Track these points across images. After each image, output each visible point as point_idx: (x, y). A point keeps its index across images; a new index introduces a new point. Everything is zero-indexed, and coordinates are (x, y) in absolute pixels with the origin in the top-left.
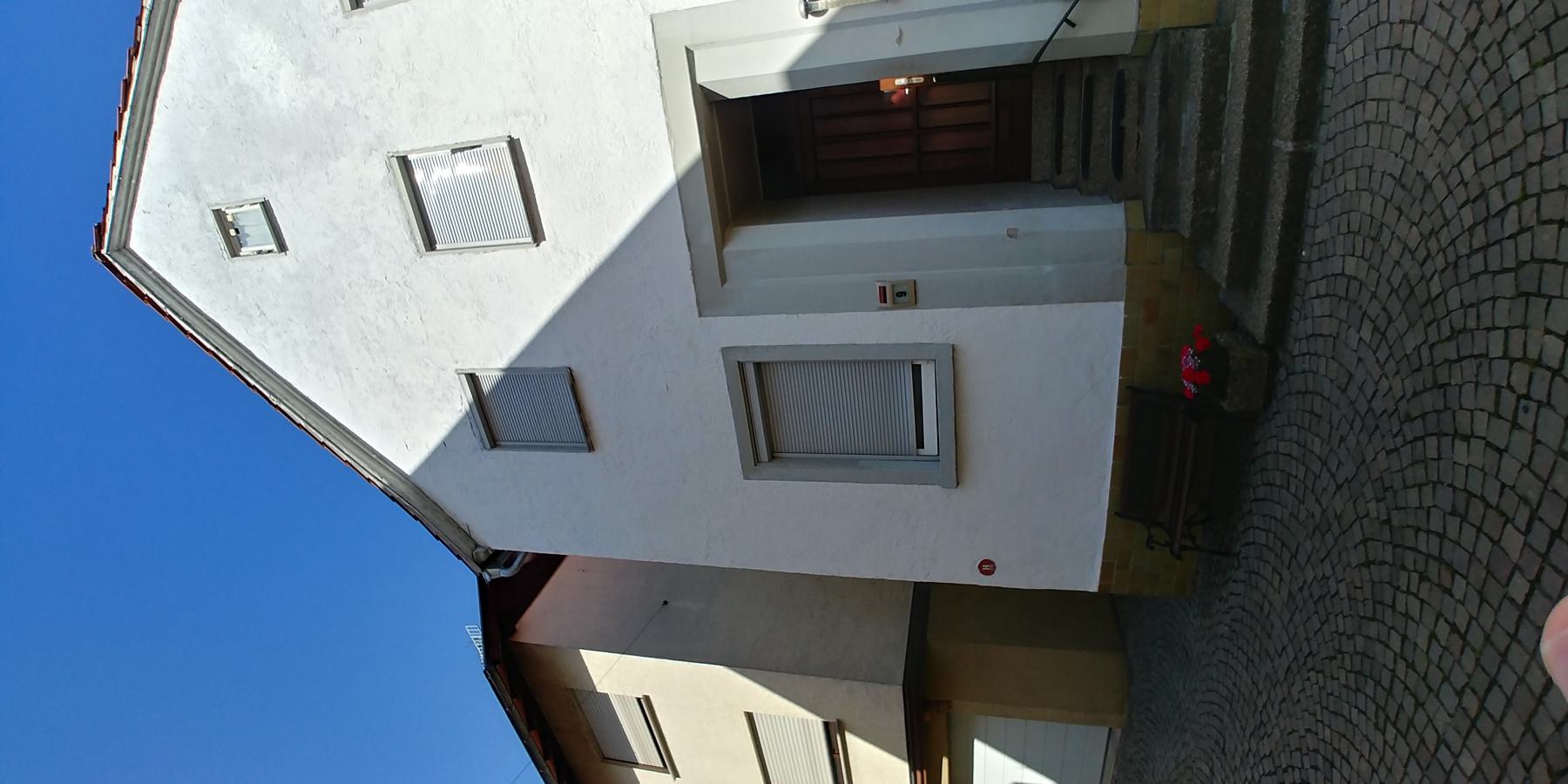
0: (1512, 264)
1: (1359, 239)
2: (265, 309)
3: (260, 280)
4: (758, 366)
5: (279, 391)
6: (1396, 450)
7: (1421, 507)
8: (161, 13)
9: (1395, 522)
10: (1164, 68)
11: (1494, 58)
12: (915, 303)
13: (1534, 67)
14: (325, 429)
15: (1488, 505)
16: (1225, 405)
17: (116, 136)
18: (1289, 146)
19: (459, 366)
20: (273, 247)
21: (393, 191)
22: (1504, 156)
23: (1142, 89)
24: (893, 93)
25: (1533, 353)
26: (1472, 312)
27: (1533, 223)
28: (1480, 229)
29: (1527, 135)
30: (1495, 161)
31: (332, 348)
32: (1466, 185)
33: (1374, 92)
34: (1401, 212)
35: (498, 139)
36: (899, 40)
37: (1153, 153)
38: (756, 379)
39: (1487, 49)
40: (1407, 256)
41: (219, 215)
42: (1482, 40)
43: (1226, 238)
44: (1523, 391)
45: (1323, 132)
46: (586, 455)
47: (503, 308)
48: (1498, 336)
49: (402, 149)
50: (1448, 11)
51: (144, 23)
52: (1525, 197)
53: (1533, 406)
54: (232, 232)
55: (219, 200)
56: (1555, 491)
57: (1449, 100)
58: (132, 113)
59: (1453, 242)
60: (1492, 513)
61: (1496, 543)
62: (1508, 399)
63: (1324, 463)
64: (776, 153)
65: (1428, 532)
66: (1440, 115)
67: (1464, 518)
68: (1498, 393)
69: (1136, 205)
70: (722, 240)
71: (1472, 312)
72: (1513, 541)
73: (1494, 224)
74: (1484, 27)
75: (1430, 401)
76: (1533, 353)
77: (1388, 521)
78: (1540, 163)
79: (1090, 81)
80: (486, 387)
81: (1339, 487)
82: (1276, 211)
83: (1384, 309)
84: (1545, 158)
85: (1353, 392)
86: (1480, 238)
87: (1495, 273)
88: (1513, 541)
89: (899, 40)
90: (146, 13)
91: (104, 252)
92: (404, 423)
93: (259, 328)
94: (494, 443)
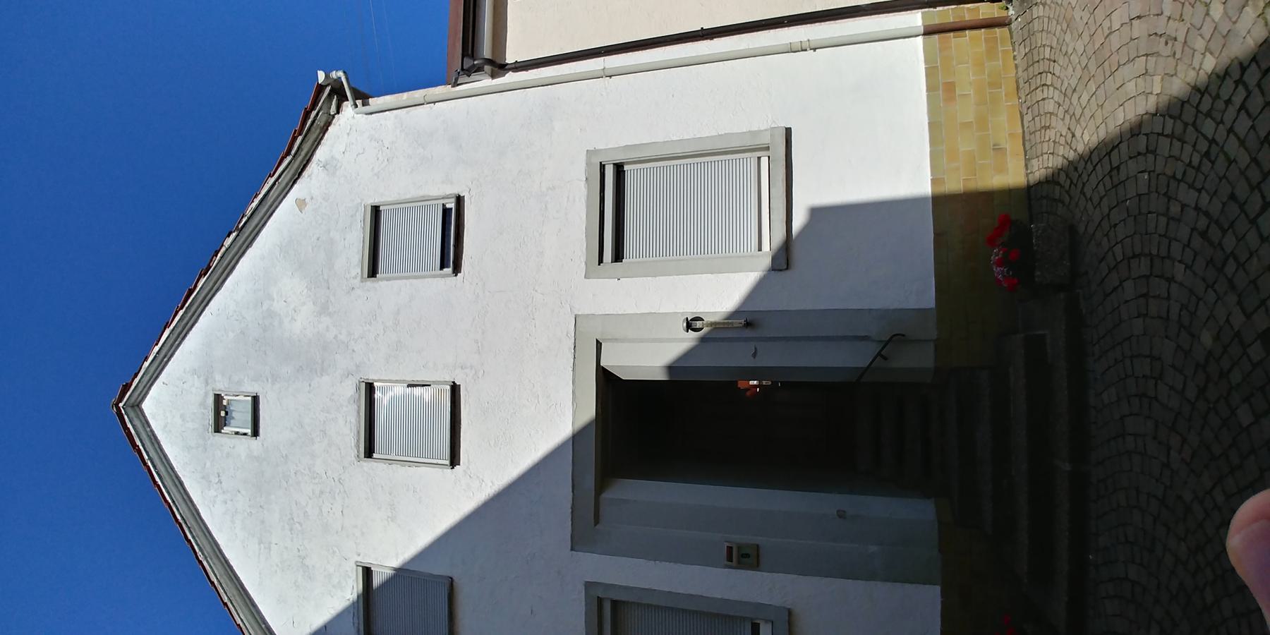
2: (223, 479)
3: (228, 455)
4: (616, 604)
5: (208, 549)
12: (756, 566)
14: (232, 592)
18: (1067, 467)
19: (359, 559)
20: (249, 431)
24: (747, 390)
31: (263, 522)
35: (445, 383)
36: (754, 355)
41: (218, 398)
47: (412, 512)
49: (371, 377)
54: (223, 414)
55: (222, 387)
70: (601, 486)
80: (377, 581)
89: (754, 355)
90: (223, 249)
93: (212, 493)
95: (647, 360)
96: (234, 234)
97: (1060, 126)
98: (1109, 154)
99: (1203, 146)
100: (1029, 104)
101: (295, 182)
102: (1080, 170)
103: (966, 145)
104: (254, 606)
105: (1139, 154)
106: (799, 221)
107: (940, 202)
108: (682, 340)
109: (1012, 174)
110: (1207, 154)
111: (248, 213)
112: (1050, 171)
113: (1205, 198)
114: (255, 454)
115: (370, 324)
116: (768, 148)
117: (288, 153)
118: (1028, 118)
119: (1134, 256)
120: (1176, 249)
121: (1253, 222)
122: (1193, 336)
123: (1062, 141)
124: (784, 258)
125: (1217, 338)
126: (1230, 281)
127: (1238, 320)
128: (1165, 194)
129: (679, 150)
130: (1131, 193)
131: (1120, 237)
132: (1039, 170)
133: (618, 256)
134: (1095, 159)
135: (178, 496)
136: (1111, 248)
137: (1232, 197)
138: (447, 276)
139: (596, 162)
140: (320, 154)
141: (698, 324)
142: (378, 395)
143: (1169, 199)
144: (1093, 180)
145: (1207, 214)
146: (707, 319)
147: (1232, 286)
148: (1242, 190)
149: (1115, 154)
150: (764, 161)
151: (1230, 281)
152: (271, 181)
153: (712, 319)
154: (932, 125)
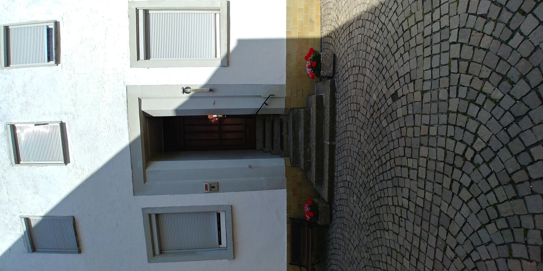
1: (350, 170)
4: (157, 215)
6: (369, 235)
7: (379, 254)
9: (372, 259)
10: (293, 119)
11: (378, 122)
12: (218, 191)
13: (388, 124)
15: (397, 252)
16: (319, 223)
18: (328, 143)
19: (22, 214)
21: (6, 138)
23: (287, 124)
25: (400, 204)
28: (380, 167)
29: (389, 142)
30: (382, 149)
33: (349, 129)
35: (56, 122)
36: (214, 104)
37: (291, 143)
38: (155, 221)
40: (363, 175)
42: (375, 116)
43: (314, 169)
44: (400, 215)
45: (337, 139)
46: (77, 255)
48: (390, 199)
49: (13, 122)
52: (391, 159)
53: (403, 220)
57: (368, 132)
60: (399, 254)
61: (402, 264)
62: (396, 218)
63: (350, 241)
64: (167, 137)
65: (382, 262)
66: (366, 136)
67: (391, 257)
68: (393, 216)
69: (288, 158)
70: (146, 166)
71: (382, 192)
72: (406, 263)
73: (384, 166)
75: (376, 219)
76: (400, 204)
77: (370, 259)
79: (273, 121)
80: (33, 224)
84: (394, 148)
85: (354, 217)
86: (381, 171)
88: (406, 263)
89: (214, 104)
94: (34, 249)
95: (166, 107)
97: (334, 14)
98: (349, 26)
99: (380, 25)
100: (324, 3)
107: (289, 41)
108: (181, 97)
109: (315, 32)
115: (9, 92)
116: (219, 10)
118: (323, 9)
119: (354, 66)
121: (393, 55)
124: (226, 61)
126: (384, 76)
127: (385, 90)
130: (355, 42)
132: (325, 33)
133: (147, 56)
134: (344, 28)
137: (388, 45)
138: (53, 65)
141: (188, 90)
142: (18, 131)
144: (343, 36)
145: (379, 51)
146: (193, 88)
148: (391, 44)
149: (351, 26)
150: (218, 15)
151: (384, 76)
153: (197, 88)
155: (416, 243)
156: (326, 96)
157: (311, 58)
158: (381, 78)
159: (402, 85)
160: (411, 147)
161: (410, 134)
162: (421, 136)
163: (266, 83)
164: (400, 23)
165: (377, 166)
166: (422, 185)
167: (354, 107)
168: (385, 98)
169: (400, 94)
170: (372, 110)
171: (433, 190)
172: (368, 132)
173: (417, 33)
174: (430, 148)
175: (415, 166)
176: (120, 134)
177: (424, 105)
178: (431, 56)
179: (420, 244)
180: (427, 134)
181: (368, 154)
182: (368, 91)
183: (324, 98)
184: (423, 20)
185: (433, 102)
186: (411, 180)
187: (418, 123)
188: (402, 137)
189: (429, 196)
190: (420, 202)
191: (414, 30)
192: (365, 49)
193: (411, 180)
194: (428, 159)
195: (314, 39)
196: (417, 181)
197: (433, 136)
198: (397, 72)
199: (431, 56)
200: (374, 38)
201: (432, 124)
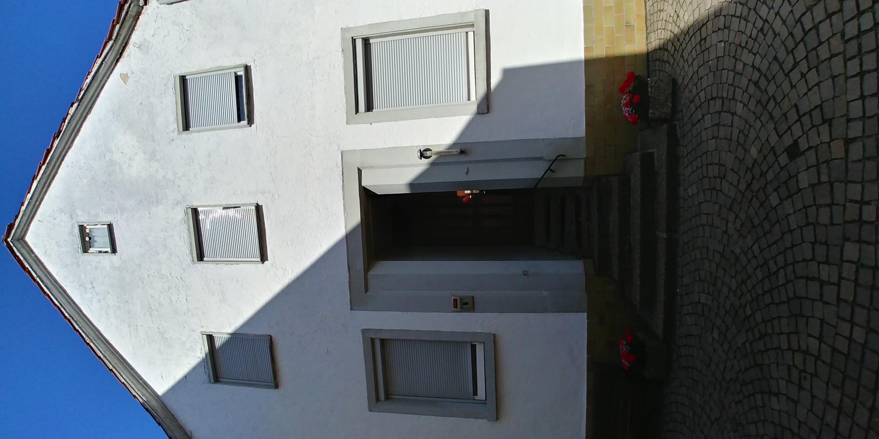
0: (785, 300)
3: (96, 268)
4: (383, 341)
5: (91, 334)
6: (740, 401)
8: (77, 118)
13: (782, 200)
14: (114, 361)
17: (34, 178)
18: (665, 236)
19: (203, 330)
20: (109, 250)
22: (773, 244)
25: (804, 347)
26: (769, 325)
27: (793, 278)
29: (783, 234)
30: (769, 246)
31: (129, 312)
32: (756, 258)
34: (725, 271)
35: (251, 204)
36: (467, 173)
38: (381, 349)
39: (758, 192)
42: (755, 186)
46: (273, 392)
47: (237, 297)
48: (784, 338)
49: (195, 204)
50: (736, 173)
51: (67, 121)
53: (808, 376)
54: (87, 239)
55: (84, 220)
56: (827, 425)
57: (743, 215)
58: (47, 167)
59: (754, 287)
62: (795, 373)
64: (393, 225)
66: (738, 224)
74: (755, 181)
78: (791, 248)
80: (218, 343)
81: (712, 423)
82: (662, 268)
83: (724, 322)
84: (793, 246)
86: (767, 286)
87: (777, 304)
89: (467, 173)
90: (69, 117)
91: (9, 240)
92: (163, 365)
93: (89, 295)
94: (216, 378)
95: (395, 179)
96: (76, 105)
98: (700, 29)
99: (759, 24)
101: (118, 61)
102: (681, 40)
103: (608, 23)
104: (132, 369)
105: (719, 29)
106: (495, 79)
107: (589, 63)
109: (637, 44)
110: (762, 29)
111: (85, 87)
112: (662, 41)
113: (758, 58)
114: (116, 265)
115: (189, 165)
116: (473, 26)
117: (110, 38)
119: (712, 99)
120: (739, 92)
121: (787, 75)
122: (746, 150)
123: (671, 20)
124: (486, 106)
125: (760, 151)
126: (770, 114)
127: (774, 139)
128: (734, 57)
129: (409, 27)
130: (713, 56)
131: (704, 86)
132: (655, 44)
133: (369, 107)
134: (691, 33)
135: (64, 301)
136: (698, 94)
137: (775, 58)
139: (349, 37)
140: (135, 38)
141: (428, 153)
143: (737, 60)
144: (689, 48)
146: (434, 150)
147: (772, 117)
148: (782, 55)
150: (471, 35)
151: (770, 114)
152: (99, 61)
154: (586, 8)
155: (830, 418)
156: (660, 152)
157: (631, 88)
158: (765, 118)
159: (806, 128)
160: (826, 243)
161: (824, 218)
162: (846, 222)
163: (550, 137)
164: (797, 16)
165: (760, 277)
166: (846, 314)
167: (713, 171)
168: (775, 154)
169: (803, 145)
170: (749, 175)
171: (868, 322)
172: (743, 215)
173: (831, 34)
174: (864, 246)
175: (835, 279)
176: (334, 220)
177: (850, 165)
178: (861, 74)
179: (838, 421)
180: (857, 218)
181: (742, 257)
182: (742, 142)
183: (655, 157)
184: (841, 10)
185: (869, 159)
186: (826, 303)
187: (839, 197)
188: (808, 224)
189: (859, 335)
190: (842, 345)
191: (825, 28)
192: (732, 68)
193: (826, 303)
194: (859, 265)
195: (635, 57)
196: (838, 306)
197: (869, 223)
198: (796, 105)
199: (861, 74)
200: (749, 46)
201: (866, 199)
